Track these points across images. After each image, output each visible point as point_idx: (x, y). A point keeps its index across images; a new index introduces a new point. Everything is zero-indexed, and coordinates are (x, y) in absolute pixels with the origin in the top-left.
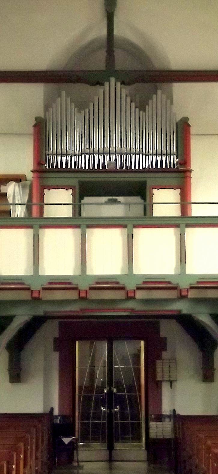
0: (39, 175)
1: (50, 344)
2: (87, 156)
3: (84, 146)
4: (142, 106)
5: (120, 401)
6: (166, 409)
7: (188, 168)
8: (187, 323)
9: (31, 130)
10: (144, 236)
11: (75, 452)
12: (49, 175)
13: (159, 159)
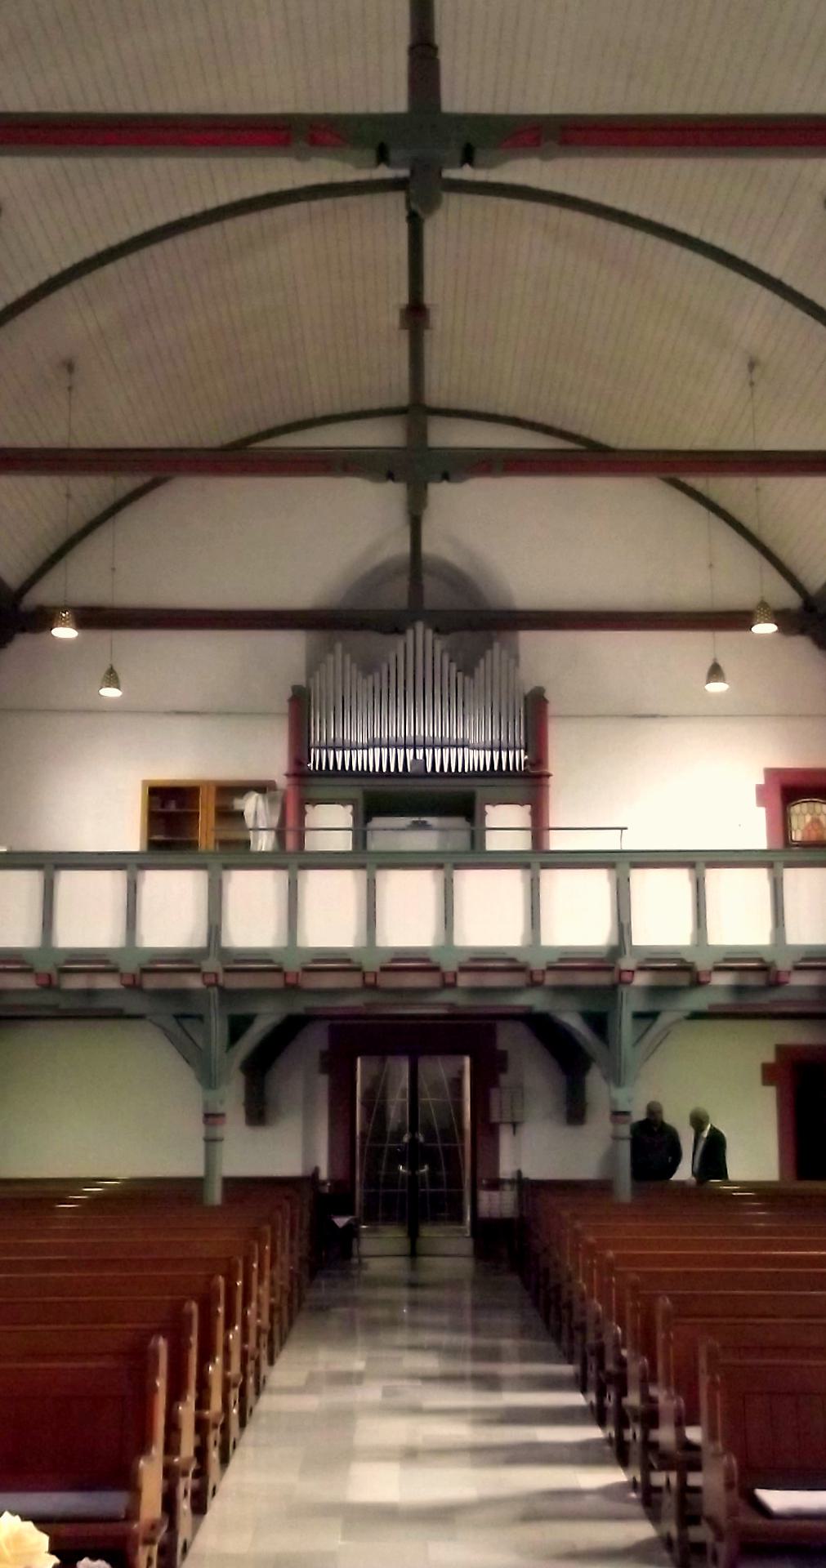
2: (385, 751)
4: (468, 669)
6: (506, 1169)
8: (543, 1027)
9: (285, 707)
10: (472, 883)
12: (315, 781)
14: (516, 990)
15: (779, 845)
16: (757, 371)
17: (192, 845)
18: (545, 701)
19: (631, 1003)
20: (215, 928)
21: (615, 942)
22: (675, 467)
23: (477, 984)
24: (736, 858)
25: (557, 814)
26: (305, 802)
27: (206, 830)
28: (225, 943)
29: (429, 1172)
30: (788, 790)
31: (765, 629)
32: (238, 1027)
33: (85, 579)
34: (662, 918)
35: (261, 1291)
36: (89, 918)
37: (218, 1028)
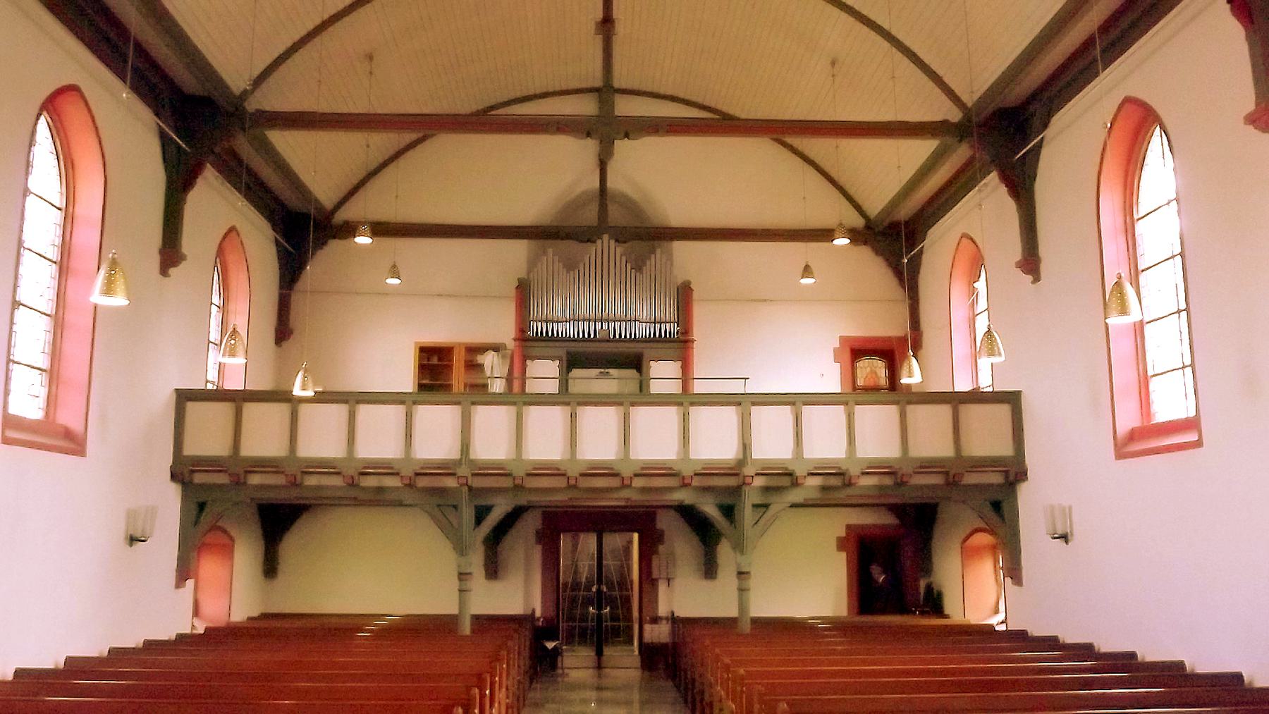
1: (532, 538)
3: (576, 309)
4: (638, 268)
5: (612, 602)
6: (663, 610)
8: (690, 515)
9: (513, 293)
10: (643, 416)
11: (559, 659)
12: (536, 344)
14: (670, 489)
15: (849, 390)
17: (447, 388)
19: (751, 497)
20: (465, 447)
21: (741, 457)
22: (780, 131)
24: (823, 399)
25: (698, 369)
26: (525, 358)
27: (458, 377)
31: (842, 242)
32: (481, 514)
33: (378, 203)
34: (773, 441)
35: (501, 695)
36: (379, 437)
37: (468, 514)
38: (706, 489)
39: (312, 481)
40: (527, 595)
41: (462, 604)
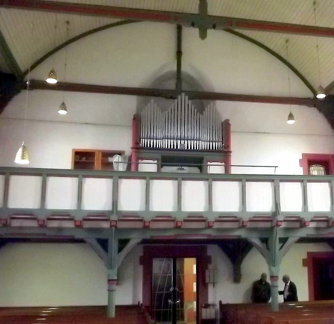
0: (137, 150)
2: (166, 140)
6: (210, 300)
7: (229, 150)
12: (143, 151)
13: (211, 144)
16: (316, 5)
18: (230, 125)
19: (279, 234)
20: (115, 203)
21: (274, 210)
23: (220, 227)
28: (119, 209)
29: (180, 302)
30: (311, 161)
36: (62, 196)
37: (114, 245)
38: (91, 230)
39: (16, 223)
40: (135, 296)
41: (110, 299)
